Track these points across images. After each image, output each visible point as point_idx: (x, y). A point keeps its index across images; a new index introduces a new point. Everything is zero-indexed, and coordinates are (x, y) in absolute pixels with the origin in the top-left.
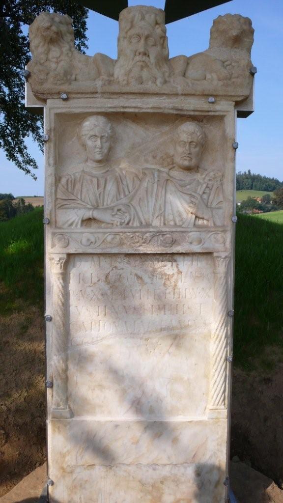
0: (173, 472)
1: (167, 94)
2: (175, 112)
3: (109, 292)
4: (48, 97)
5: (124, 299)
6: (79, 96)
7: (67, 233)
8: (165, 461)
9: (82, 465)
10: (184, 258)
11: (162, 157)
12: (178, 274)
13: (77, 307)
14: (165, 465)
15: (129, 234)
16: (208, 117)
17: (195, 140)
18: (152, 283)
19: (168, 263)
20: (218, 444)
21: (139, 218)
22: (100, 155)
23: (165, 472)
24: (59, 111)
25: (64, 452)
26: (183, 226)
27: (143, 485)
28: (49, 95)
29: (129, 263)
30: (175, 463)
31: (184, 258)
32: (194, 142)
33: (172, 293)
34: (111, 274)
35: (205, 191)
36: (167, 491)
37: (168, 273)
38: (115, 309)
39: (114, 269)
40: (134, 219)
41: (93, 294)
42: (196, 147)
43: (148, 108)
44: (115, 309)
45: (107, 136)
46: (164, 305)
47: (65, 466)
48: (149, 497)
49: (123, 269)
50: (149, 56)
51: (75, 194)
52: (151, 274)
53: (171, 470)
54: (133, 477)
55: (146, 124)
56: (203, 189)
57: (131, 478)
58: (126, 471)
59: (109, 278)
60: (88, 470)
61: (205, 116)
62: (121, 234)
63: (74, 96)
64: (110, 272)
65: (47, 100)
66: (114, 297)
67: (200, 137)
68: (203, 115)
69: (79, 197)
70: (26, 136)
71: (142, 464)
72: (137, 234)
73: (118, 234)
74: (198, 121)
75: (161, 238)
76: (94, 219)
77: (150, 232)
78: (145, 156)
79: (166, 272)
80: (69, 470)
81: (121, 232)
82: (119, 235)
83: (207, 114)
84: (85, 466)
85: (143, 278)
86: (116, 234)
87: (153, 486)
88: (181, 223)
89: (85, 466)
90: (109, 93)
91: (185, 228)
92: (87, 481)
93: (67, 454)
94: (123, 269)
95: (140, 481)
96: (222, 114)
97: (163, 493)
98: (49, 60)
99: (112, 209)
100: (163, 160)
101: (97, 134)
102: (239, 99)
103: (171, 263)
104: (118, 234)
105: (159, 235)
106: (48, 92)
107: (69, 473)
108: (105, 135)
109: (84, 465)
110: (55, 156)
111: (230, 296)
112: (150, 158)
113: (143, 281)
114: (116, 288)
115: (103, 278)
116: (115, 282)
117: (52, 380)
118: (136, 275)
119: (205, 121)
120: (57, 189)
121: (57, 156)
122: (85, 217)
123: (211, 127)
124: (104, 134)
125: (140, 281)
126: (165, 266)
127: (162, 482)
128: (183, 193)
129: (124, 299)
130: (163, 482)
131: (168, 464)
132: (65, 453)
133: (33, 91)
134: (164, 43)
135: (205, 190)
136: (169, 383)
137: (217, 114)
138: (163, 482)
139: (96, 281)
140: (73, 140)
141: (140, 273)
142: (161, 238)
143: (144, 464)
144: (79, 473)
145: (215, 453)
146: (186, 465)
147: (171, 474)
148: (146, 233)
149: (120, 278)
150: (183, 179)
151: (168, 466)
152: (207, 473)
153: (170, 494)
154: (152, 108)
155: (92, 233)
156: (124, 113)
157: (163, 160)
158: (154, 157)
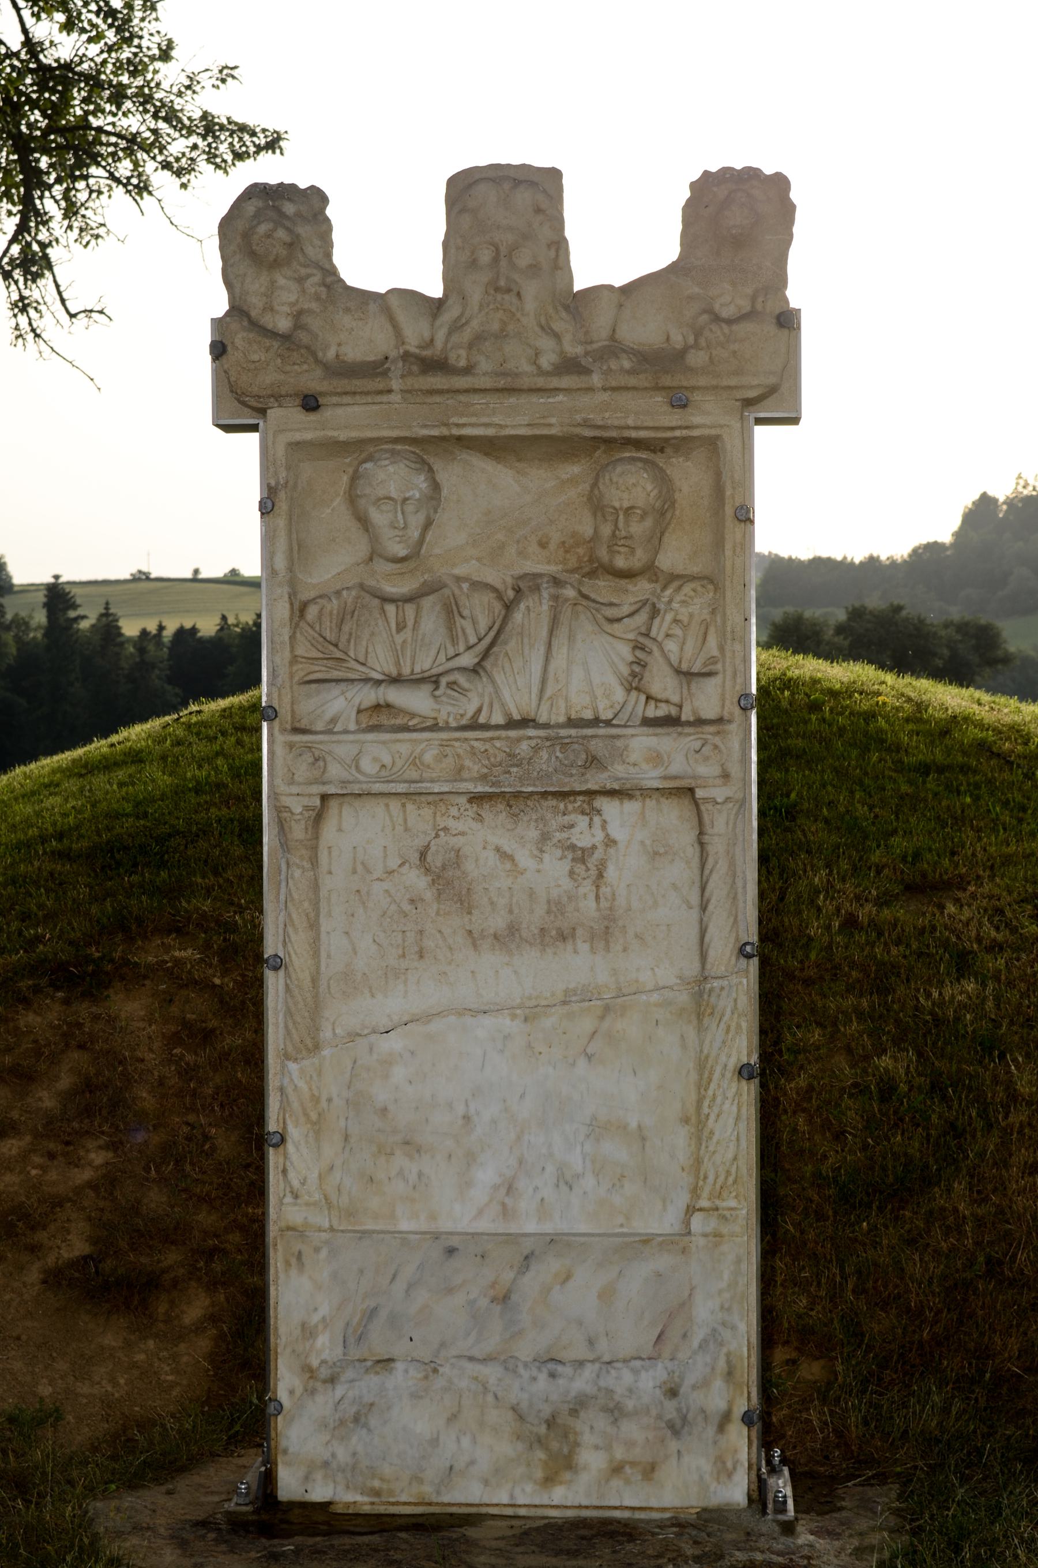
0: (602, 1383)
1: (565, 390)
2: (588, 433)
3: (428, 895)
4: (270, 405)
5: (470, 913)
6: (347, 399)
7: (321, 742)
8: (580, 1351)
9: (358, 1360)
10: (622, 803)
11: (563, 543)
12: (607, 845)
13: (347, 933)
14: (580, 1364)
15: (476, 744)
16: (673, 441)
17: (640, 503)
18: (538, 871)
19: (580, 817)
20: (722, 1307)
21: (503, 705)
22: (402, 545)
23: (582, 1382)
24: (298, 437)
25: (312, 1324)
26: (614, 722)
27: (521, 1418)
28: (272, 400)
29: (479, 818)
30: (607, 1358)
31: (622, 803)
32: (639, 508)
33: (592, 896)
34: (433, 848)
35: (670, 632)
36: (587, 1438)
37: (580, 844)
38: (445, 940)
39: (442, 833)
40: (491, 705)
41: (389, 899)
42: (643, 517)
43: (520, 425)
44: (445, 940)
45: (417, 496)
46: (574, 929)
47: (315, 1363)
48: (541, 1455)
49: (463, 834)
50: (518, 294)
51: (341, 646)
52: (538, 848)
53: (598, 1376)
54: (496, 1397)
55: (519, 460)
56: (666, 625)
57: (490, 1398)
58: (476, 1379)
59: (429, 858)
60: (377, 1373)
61: (667, 440)
62: (457, 744)
63: (335, 399)
64: (433, 843)
65: (269, 411)
66: (442, 907)
67: (652, 494)
68: (659, 439)
69: (352, 654)
70: (60, 17)
71: (517, 1358)
72: (498, 744)
73: (449, 743)
74: (651, 450)
75: (558, 754)
76: (388, 706)
77: (530, 738)
78: (518, 542)
79: (575, 842)
80: (324, 1373)
81: (457, 740)
82: (452, 746)
83: (669, 434)
84: (369, 1364)
85: (517, 858)
86: (444, 743)
87: (551, 1423)
88: (610, 716)
89: (369, 1364)
90: (421, 390)
91: (618, 726)
92: (372, 1405)
93: (321, 1327)
94: (463, 834)
95: (513, 1409)
96: (713, 432)
97: (577, 1444)
98: (272, 310)
99: (434, 681)
100: (566, 552)
101: (394, 495)
102: (752, 394)
103: (587, 818)
104: (449, 743)
105: (553, 745)
106: (269, 392)
107: (325, 1382)
108: (414, 495)
109: (365, 1360)
110: (291, 550)
111: (272, 651)
112: (533, 548)
113: (516, 865)
114: (449, 883)
115: (415, 857)
116: (444, 867)
117: (285, 1128)
118: (498, 849)
119: (669, 451)
120: (295, 633)
121: (296, 548)
122: (367, 704)
123: (689, 463)
124: (411, 493)
125: (508, 866)
126: (572, 826)
127: (574, 1412)
128: (613, 636)
129: (470, 913)
130: (576, 1411)
131: (589, 1361)
132: (316, 1326)
133: (232, 391)
134: (557, 256)
135: (669, 629)
136: (588, 1136)
137: (696, 433)
138: (576, 1411)
139: (395, 867)
140: (335, 504)
141: (508, 845)
142: (558, 754)
143: (523, 1359)
144: (352, 1381)
145: (714, 1330)
146: (638, 1363)
147: (599, 1389)
148: (519, 740)
149: (457, 857)
150: (615, 601)
151: (589, 1365)
152: (694, 1387)
153: (597, 1447)
154: (528, 425)
155: (384, 743)
156: (459, 439)
157: (566, 552)
158: (543, 545)
